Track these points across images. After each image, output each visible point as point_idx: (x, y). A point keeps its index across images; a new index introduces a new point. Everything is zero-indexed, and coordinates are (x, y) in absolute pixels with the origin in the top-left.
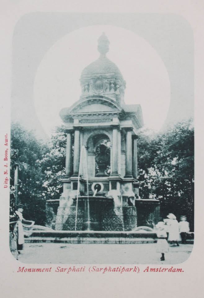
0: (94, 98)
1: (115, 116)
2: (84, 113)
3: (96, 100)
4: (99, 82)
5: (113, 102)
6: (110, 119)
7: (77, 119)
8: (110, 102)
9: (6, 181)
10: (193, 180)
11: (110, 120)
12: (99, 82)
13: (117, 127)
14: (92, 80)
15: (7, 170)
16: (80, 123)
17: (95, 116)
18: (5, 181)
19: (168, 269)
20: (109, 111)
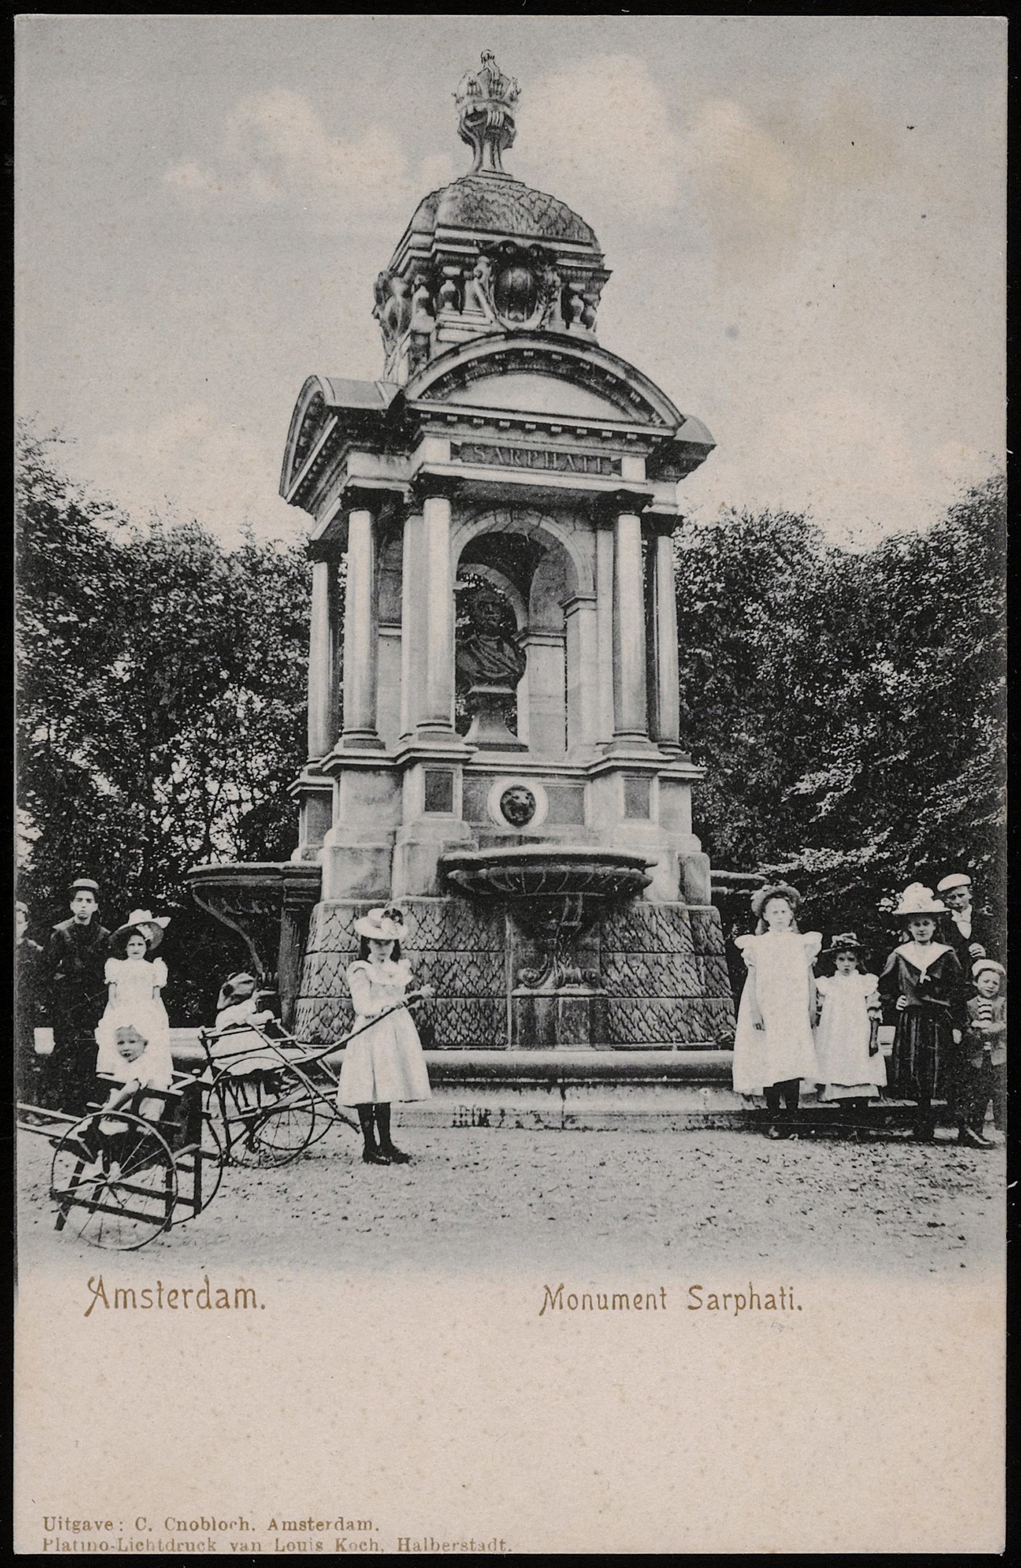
0: (542, 346)
1: (640, 448)
2: (514, 412)
3: (518, 353)
4: (518, 277)
5: (641, 382)
6: (609, 459)
7: (437, 435)
8: (622, 375)
9: (71, 1525)
10: (801, 792)
11: (608, 468)
12: (518, 277)
13: (632, 501)
14: (484, 259)
15: (263, 1307)
16: (458, 461)
17: (590, 442)
18: (71, 1520)
19: (191, 1291)
20: (601, 416)
